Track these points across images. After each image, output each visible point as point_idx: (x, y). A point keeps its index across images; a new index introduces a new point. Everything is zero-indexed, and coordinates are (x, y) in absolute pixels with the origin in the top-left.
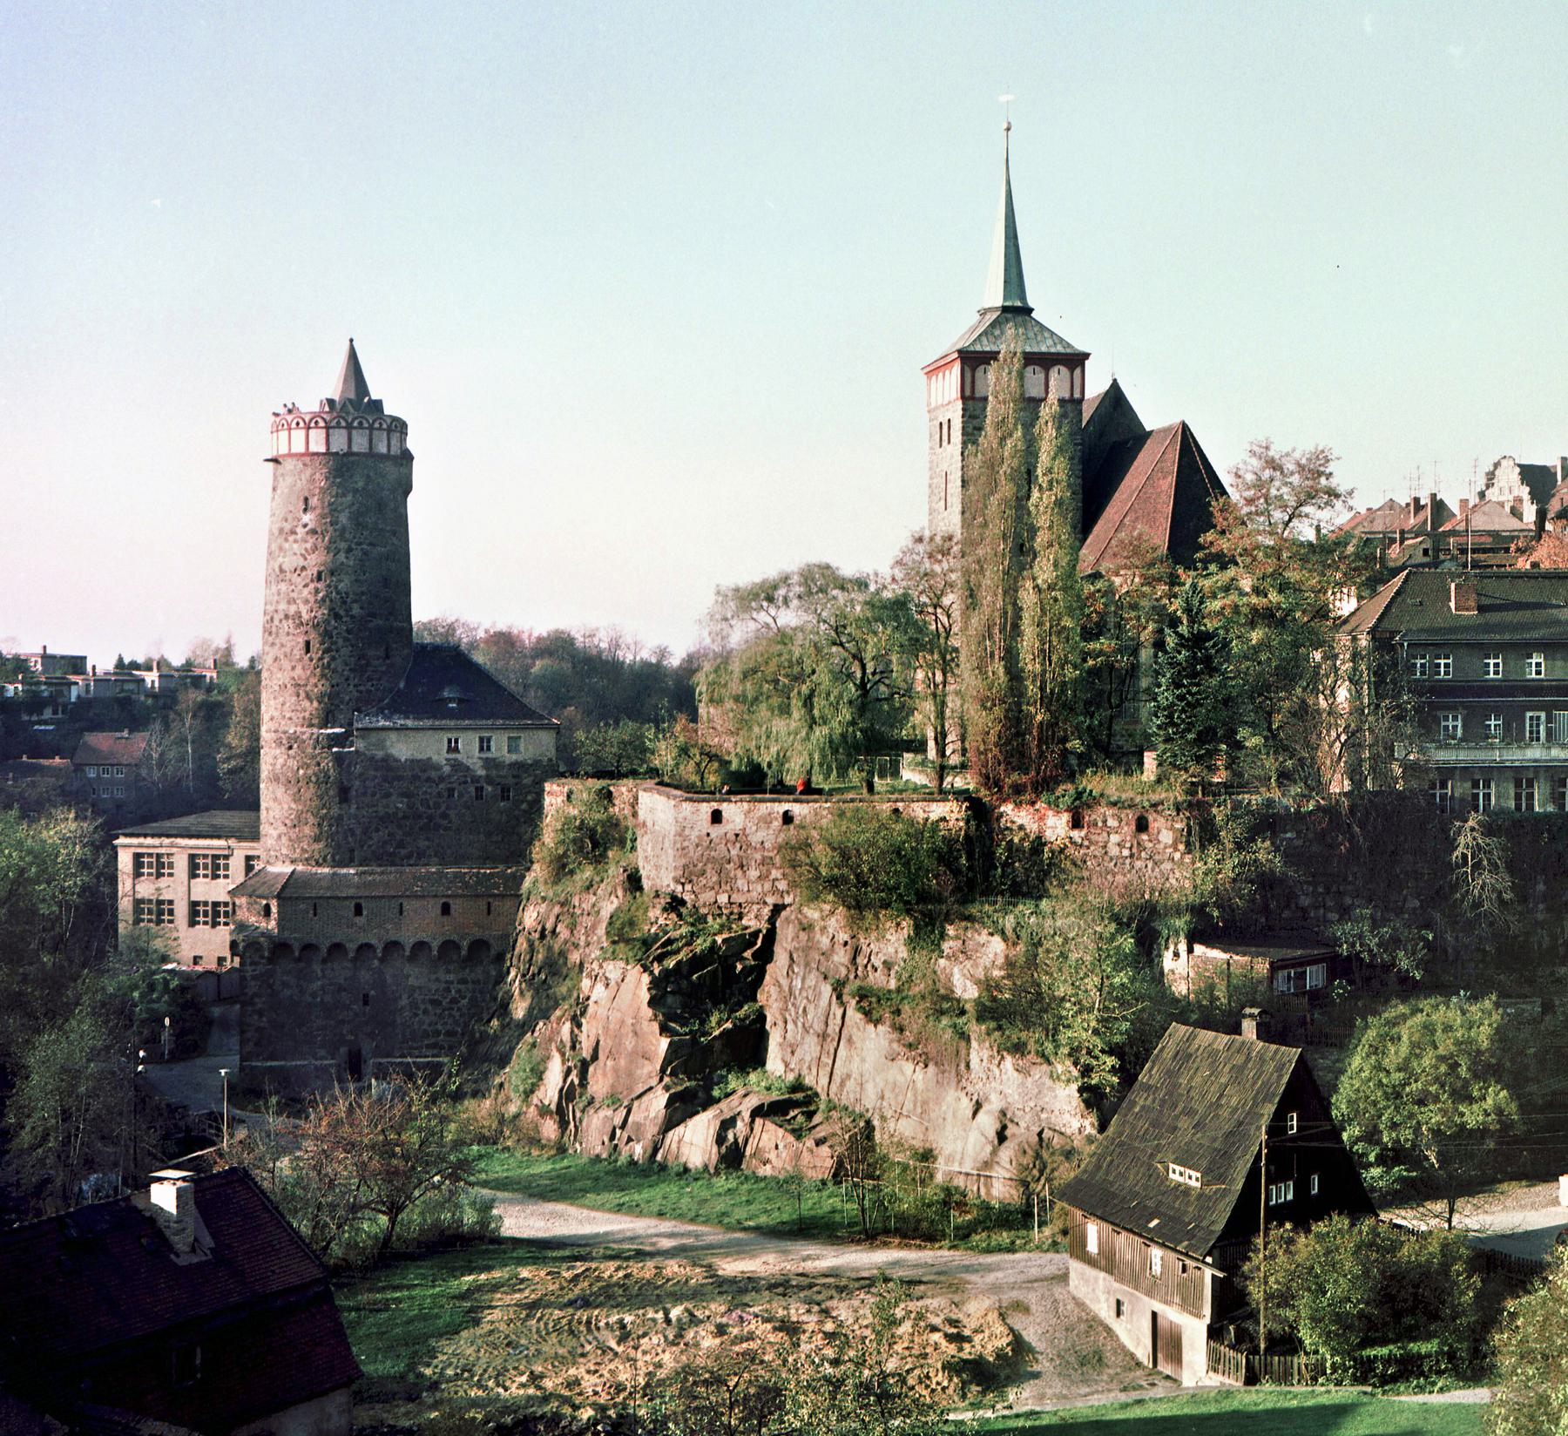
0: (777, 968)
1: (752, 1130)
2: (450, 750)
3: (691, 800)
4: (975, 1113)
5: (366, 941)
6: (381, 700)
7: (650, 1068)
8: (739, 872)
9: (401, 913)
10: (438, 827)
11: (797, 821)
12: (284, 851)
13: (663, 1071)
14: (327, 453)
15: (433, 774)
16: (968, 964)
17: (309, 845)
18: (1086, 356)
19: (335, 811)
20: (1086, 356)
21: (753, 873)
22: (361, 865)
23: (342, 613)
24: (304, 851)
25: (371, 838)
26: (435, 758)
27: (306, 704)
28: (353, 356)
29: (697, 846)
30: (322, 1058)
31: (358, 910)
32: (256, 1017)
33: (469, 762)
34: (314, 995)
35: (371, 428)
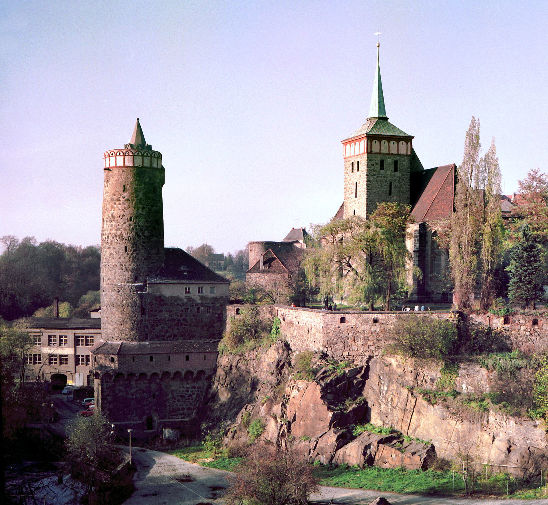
0: (372, 380)
1: (378, 449)
2: (186, 292)
3: (331, 313)
4: (493, 441)
5: (154, 371)
6: (156, 271)
7: (324, 424)
8: (353, 343)
9: (169, 360)
10: (182, 324)
11: (380, 321)
12: (117, 335)
13: (330, 425)
14: (133, 167)
15: (180, 303)
16: (470, 379)
17: (128, 332)
18: (413, 137)
19: (140, 318)
20: (413, 137)
21: (360, 343)
22: (150, 340)
23: (141, 235)
25: (154, 329)
26: (180, 296)
27: (126, 273)
29: (334, 332)
30: (136, 421)
31: (151, 359)
32: (108, 405)
33: (194, 298)
34: (132, 394)
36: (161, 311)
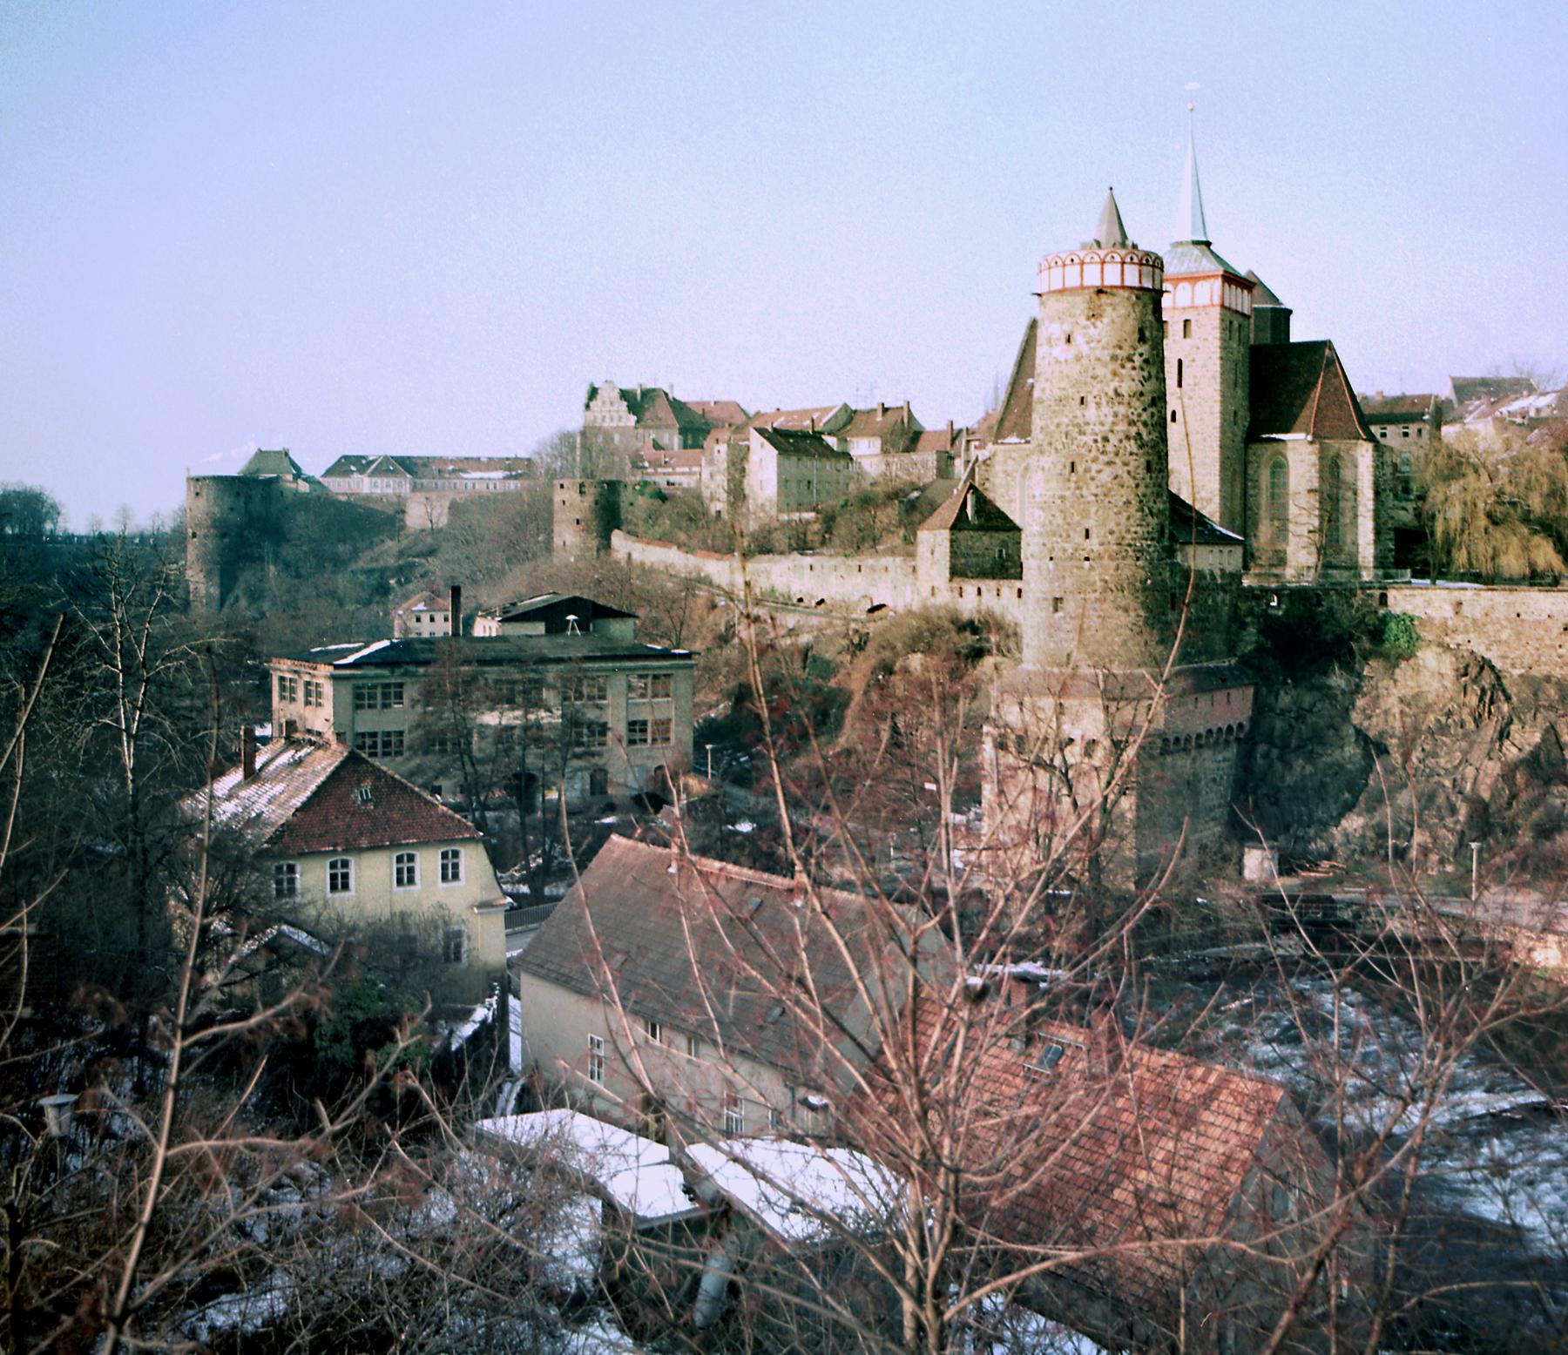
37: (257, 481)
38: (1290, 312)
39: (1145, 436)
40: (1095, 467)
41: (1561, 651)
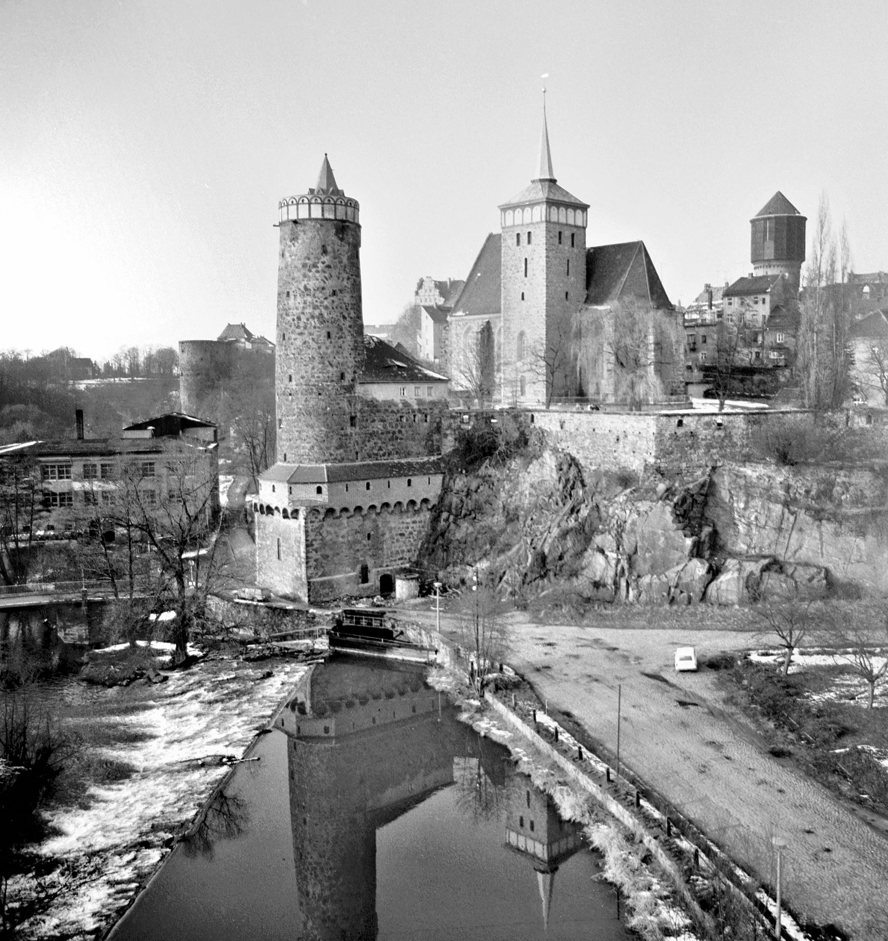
10: (397, 438)
15: (395, 409)
18: (589, 206)
20: (589, 206)
24: (331, 455)
28: (327, 162)
33: (410, 401)
34: (343, 537)
35: (335, 204)
36: (374, 421)
37: (223, 343)
38: (805, 219)
39: (325, 315)
40: (293, 336)
41: (615, 454)
